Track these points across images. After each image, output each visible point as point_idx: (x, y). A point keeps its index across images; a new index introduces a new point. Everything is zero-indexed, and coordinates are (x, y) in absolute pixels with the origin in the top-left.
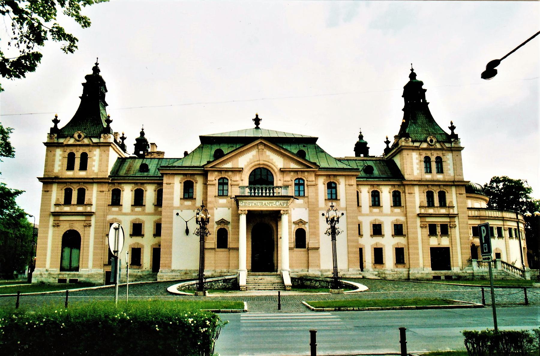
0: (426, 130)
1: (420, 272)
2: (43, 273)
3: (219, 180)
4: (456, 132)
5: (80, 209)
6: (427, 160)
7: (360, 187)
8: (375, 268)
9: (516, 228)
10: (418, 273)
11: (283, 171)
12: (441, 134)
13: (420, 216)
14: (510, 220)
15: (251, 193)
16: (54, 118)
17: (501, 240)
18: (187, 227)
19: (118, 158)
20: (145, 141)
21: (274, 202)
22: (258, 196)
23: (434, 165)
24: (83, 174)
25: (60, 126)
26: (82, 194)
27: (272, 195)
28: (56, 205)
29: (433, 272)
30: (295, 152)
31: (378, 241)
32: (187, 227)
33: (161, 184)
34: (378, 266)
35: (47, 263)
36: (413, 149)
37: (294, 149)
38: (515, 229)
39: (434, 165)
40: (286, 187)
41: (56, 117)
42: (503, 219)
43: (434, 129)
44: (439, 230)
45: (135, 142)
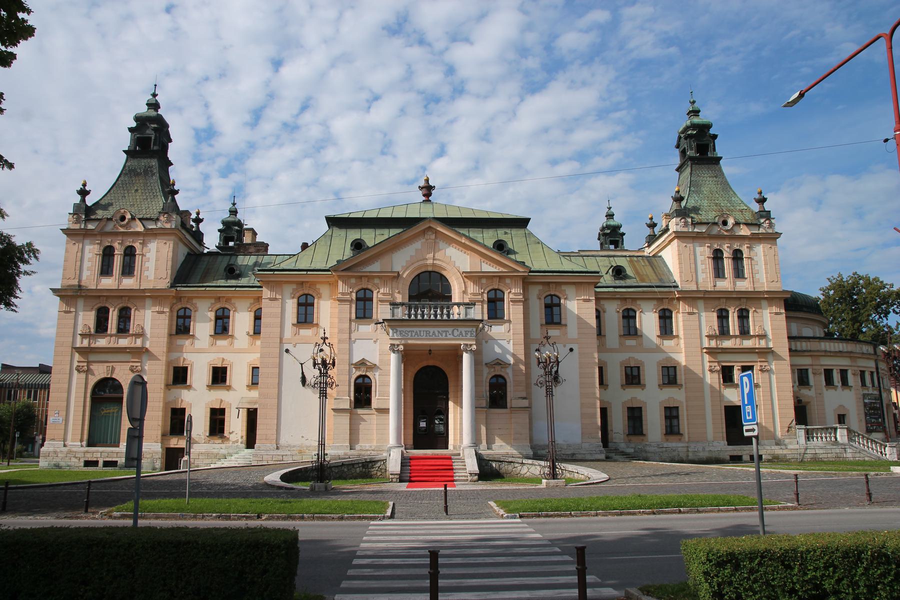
0: (716, 205)
1: (707, 449)
2: (58, 450)
3: (357, 293)
4: (767, 206)
5: (124, 342)
6: (717, 256)
7: (602, 302)
8: (630, 441)
9: (874, 370)
10: (704, 449)
11: (469, 276)
12: (741, 211)
13: (711, 352)
14: (864, 356)
15: (410, 315)
16: (79, 187)
17: (847, 391)
18: (303, 373)
19: (188, 254)
20: (239, 224)
21: (450, 330)
22: (442, 320)
23: (728, 264)
24: (128, 283)
25: (90, 201)
26: (125, 317)
27: (445, 317)
28: (83, 336)
29: (731, 447)
30: (490, 243)
31: (634, 395)
32: (303, 373)
33: (259, 299)
34: (634, 438)
35: (64, 446)
36: (693, 238)
37: (489, 237)
38: (872, 373)
39: (728, 264)
40: (469, 305)
41: (84, 185)
42: (849, 355)
43: (730, 202)
44: (836, 377)
45: (221, 227)
